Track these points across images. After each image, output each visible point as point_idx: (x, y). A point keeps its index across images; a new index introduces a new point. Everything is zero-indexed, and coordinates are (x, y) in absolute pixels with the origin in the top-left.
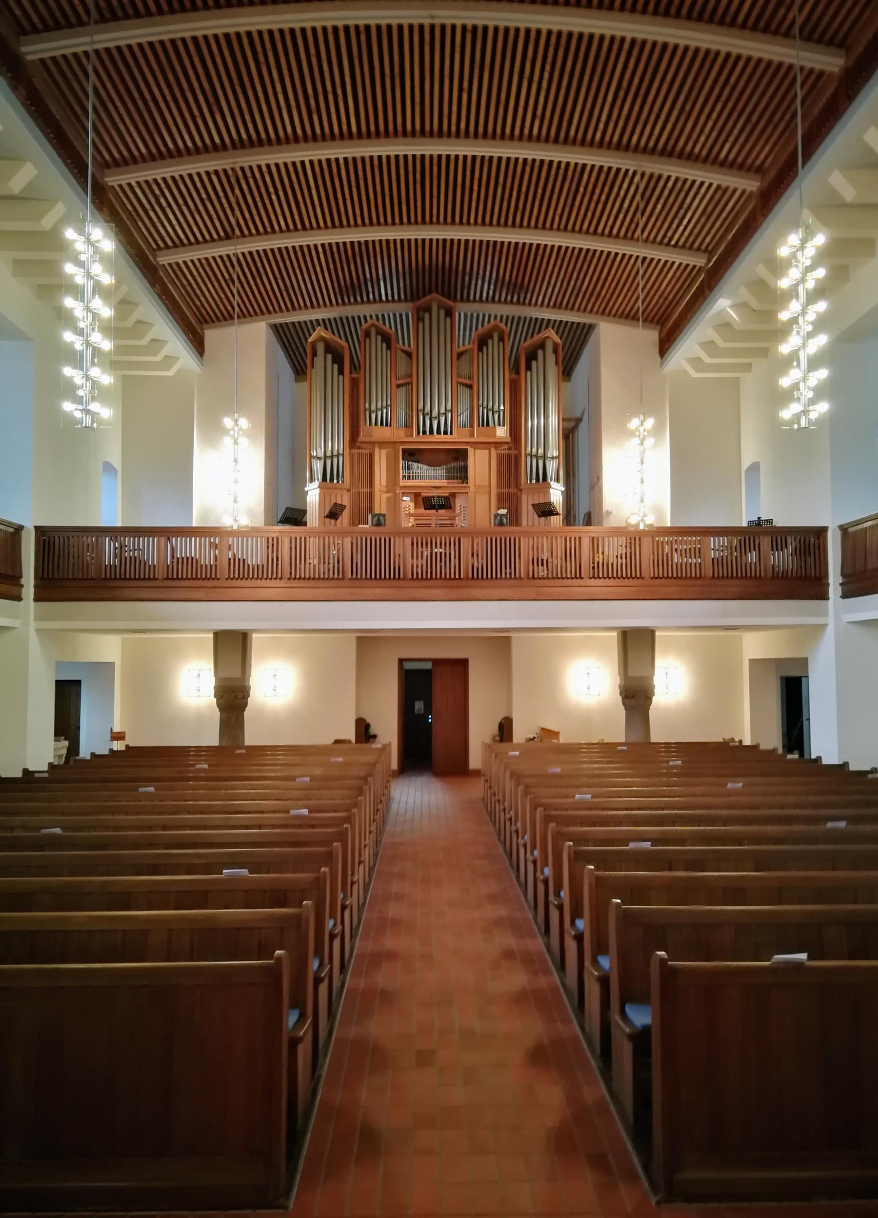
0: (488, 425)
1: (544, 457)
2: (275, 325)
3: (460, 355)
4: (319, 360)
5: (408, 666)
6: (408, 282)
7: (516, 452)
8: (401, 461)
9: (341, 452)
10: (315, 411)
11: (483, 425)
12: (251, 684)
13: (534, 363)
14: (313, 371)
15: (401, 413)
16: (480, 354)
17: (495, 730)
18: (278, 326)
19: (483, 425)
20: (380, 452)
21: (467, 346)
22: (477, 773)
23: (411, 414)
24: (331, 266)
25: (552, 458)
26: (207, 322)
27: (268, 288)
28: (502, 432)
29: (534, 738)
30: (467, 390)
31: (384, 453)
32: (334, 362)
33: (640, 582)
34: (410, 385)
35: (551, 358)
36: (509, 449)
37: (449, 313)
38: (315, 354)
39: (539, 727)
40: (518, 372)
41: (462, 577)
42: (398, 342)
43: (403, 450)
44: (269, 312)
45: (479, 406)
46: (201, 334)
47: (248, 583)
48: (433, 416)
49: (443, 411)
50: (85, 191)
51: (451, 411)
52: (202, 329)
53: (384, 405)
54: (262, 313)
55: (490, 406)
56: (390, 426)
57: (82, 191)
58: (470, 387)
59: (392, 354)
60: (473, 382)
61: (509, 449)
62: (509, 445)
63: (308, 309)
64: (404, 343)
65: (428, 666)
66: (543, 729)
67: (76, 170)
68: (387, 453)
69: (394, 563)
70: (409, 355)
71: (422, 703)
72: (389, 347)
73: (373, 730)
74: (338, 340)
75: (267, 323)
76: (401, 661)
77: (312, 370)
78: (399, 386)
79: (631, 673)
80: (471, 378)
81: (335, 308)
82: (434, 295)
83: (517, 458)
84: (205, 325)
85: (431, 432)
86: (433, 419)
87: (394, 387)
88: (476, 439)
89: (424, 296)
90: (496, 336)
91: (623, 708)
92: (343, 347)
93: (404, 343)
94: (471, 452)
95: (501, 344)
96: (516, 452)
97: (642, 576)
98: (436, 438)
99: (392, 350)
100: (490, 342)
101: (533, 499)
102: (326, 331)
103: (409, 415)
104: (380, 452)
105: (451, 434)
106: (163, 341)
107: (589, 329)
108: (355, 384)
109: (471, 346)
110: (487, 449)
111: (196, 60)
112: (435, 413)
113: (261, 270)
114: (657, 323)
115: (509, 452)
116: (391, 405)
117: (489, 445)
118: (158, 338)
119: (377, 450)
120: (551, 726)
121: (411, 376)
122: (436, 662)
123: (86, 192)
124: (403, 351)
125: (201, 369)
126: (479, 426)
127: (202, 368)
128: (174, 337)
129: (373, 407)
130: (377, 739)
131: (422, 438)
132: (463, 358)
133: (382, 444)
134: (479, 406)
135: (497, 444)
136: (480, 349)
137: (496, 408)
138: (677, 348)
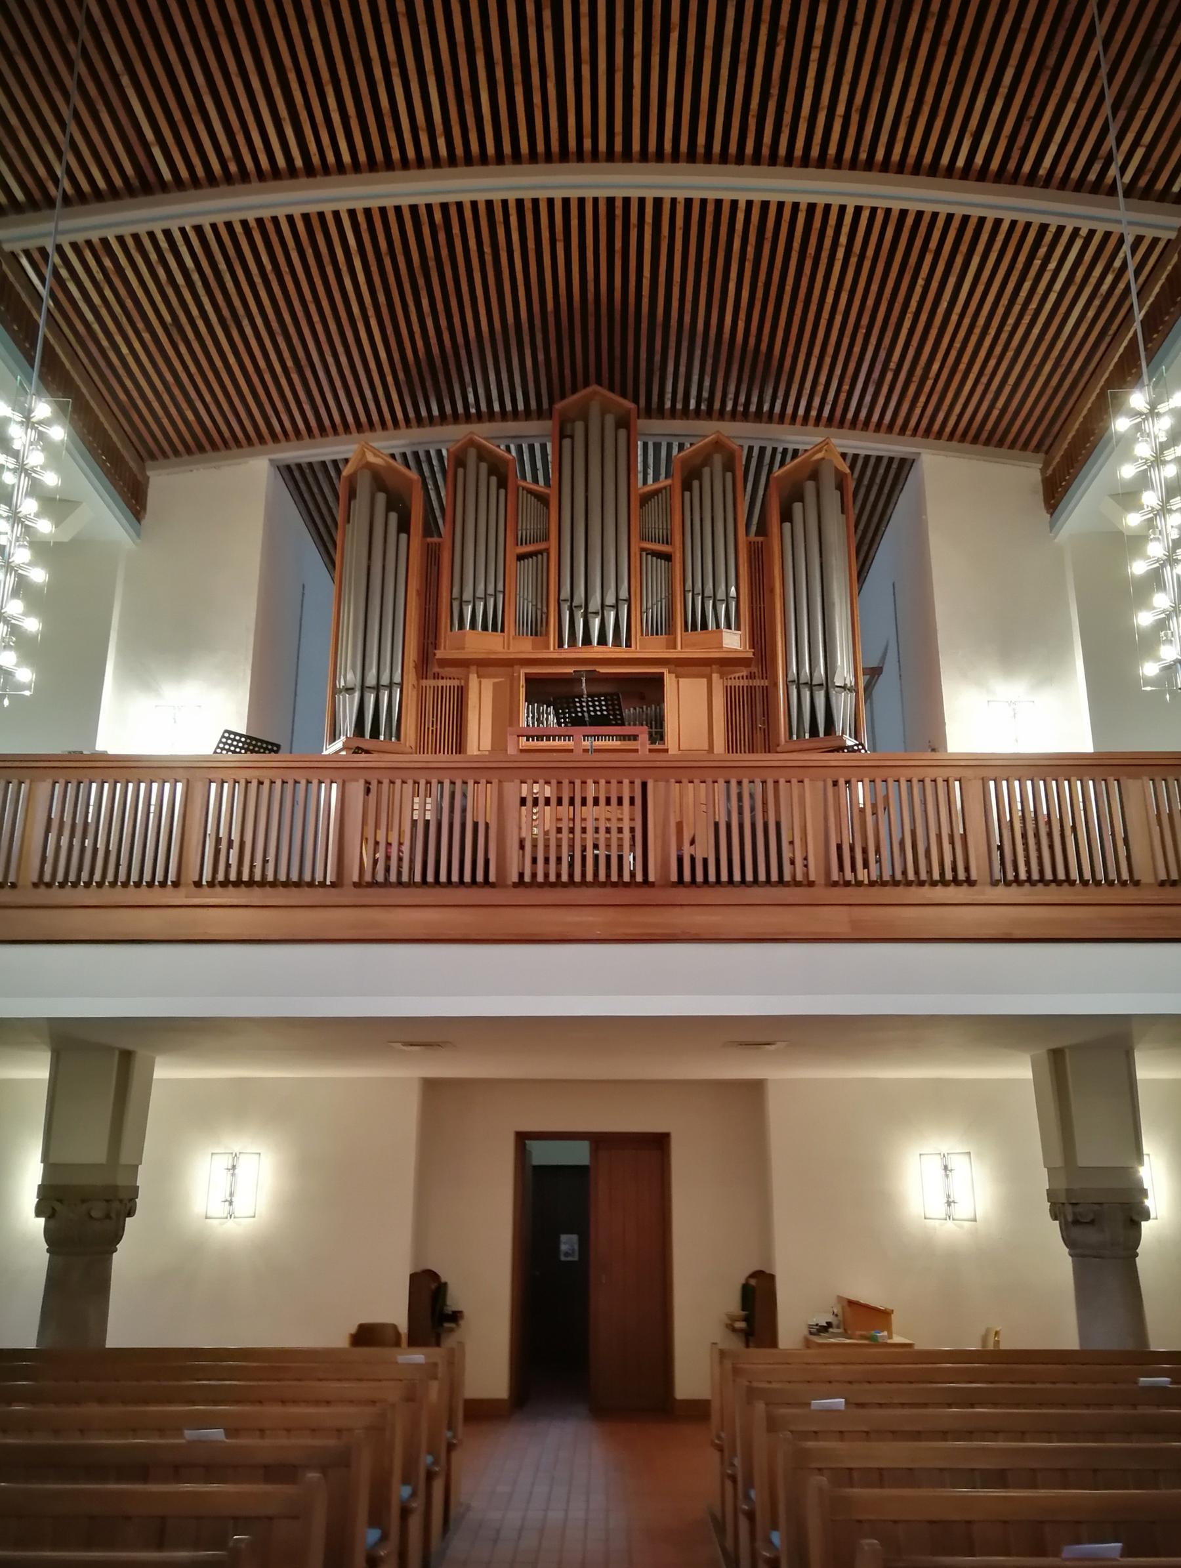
0: (704, 626)
1: (827, 685)
2: (288, 467)
3: (645, 499)
4: (361, 506)
5: (544, 1154)
6: (541, 357)
7: (765, 683)
8: (523, 705)
9: (397, 679)
10: (346, 611)
11: (694, 628)
12: (42, 1164)
13: (797, 507)
14: (349, 527)
15: (524, 602)
16: (687, 494)
17: (732, 1303)
18: (294, 467)
19: (694, 628)
20: (480, 683)
21: (663, 482)
22: (698, 1411)
23: (545, 610)
24: (382, 298)
25: (844, 687)
26: (153, 457)
27: (262, 364)
28: (733, 641)
29: (829, 1325)
30: (662, 563)
31: (488, 685)
32: (389, 508)
33: (1130, 894)
34: (545, 554)
35: (832, 499)
36: (751, 676)
37: (623, 423)
38: (352, 495)
39: (840, 1298)
40: (762, 530)
41: (651, 878)
42: (524, 478)
43: (530, 680)
45: (685, 592)
46: (139, 477)
47: (91, 896)
48: (591, 609)
49: (610, 600)
50: (31, 361)
51: (629, 601)
52: (143, 470)
53: (491, 590)
55: (709, 590)
56: (502, 631)
57: (26, 363)
58: (668, 557)
61: (751, 676)
62: (749, 669)
63: (350, 433)
64: (535, 480)
65: (579, 1154)
66: (851, 1303)
67: (108, 465)
68: (495, 685)
69: (464, 810)
70: (543, 499)
71: (574, 1238)
72: (502, 484)
73: (457, 1298)
74: (403, 469)
75: (271, 461)
76: (522, 1138)
77: (347, 526)
78: (521, 557)
79: (1085, 1159)
80: (668, 541)
81: (404, 430)
82: (594, 387)
83: (768, 695)
84: (149, 463)
85: (587, 640)
86: (589, 615)
87: (511, 558)
88: (678, 653)
89: (574, 390)
90: (718, 460)
91: (1066, 1250)
92: (410, 480)
93: (535, 480)
94: (669, 680)
96: (765, 683)
97: (1136, 877)
98: (596, 651)
99: (509, 490)
100: (706, 471)
101: (1029, 119)
103: (542, 613)
104: (480, 683)
105: (628, 645)
106: (69, 501)
107: (903, 467)
108: (432, 557)
110: (702, 676)
112: (595, 604)
113: (241, 311)
114: (1037, 449)
115: (750, 683)
116: (504, 592)
117: (707, 670)
118: (71, 499)
119: (473, 680)
120: (869, 1294)
121: (546, 538)
122: (599, 1141)
123: (32, 367)
124: (530, 492)
126: (686, 629)
127: (139, 541)
129: (468, 595)
130: (462, 1323)
131: (567, 653)
132: (654, 501)
133: (484, 665)
134: (685, 592)
135: (727, 663)
136: (687, 486)
137: (721, 594)
138: (1093, 471)
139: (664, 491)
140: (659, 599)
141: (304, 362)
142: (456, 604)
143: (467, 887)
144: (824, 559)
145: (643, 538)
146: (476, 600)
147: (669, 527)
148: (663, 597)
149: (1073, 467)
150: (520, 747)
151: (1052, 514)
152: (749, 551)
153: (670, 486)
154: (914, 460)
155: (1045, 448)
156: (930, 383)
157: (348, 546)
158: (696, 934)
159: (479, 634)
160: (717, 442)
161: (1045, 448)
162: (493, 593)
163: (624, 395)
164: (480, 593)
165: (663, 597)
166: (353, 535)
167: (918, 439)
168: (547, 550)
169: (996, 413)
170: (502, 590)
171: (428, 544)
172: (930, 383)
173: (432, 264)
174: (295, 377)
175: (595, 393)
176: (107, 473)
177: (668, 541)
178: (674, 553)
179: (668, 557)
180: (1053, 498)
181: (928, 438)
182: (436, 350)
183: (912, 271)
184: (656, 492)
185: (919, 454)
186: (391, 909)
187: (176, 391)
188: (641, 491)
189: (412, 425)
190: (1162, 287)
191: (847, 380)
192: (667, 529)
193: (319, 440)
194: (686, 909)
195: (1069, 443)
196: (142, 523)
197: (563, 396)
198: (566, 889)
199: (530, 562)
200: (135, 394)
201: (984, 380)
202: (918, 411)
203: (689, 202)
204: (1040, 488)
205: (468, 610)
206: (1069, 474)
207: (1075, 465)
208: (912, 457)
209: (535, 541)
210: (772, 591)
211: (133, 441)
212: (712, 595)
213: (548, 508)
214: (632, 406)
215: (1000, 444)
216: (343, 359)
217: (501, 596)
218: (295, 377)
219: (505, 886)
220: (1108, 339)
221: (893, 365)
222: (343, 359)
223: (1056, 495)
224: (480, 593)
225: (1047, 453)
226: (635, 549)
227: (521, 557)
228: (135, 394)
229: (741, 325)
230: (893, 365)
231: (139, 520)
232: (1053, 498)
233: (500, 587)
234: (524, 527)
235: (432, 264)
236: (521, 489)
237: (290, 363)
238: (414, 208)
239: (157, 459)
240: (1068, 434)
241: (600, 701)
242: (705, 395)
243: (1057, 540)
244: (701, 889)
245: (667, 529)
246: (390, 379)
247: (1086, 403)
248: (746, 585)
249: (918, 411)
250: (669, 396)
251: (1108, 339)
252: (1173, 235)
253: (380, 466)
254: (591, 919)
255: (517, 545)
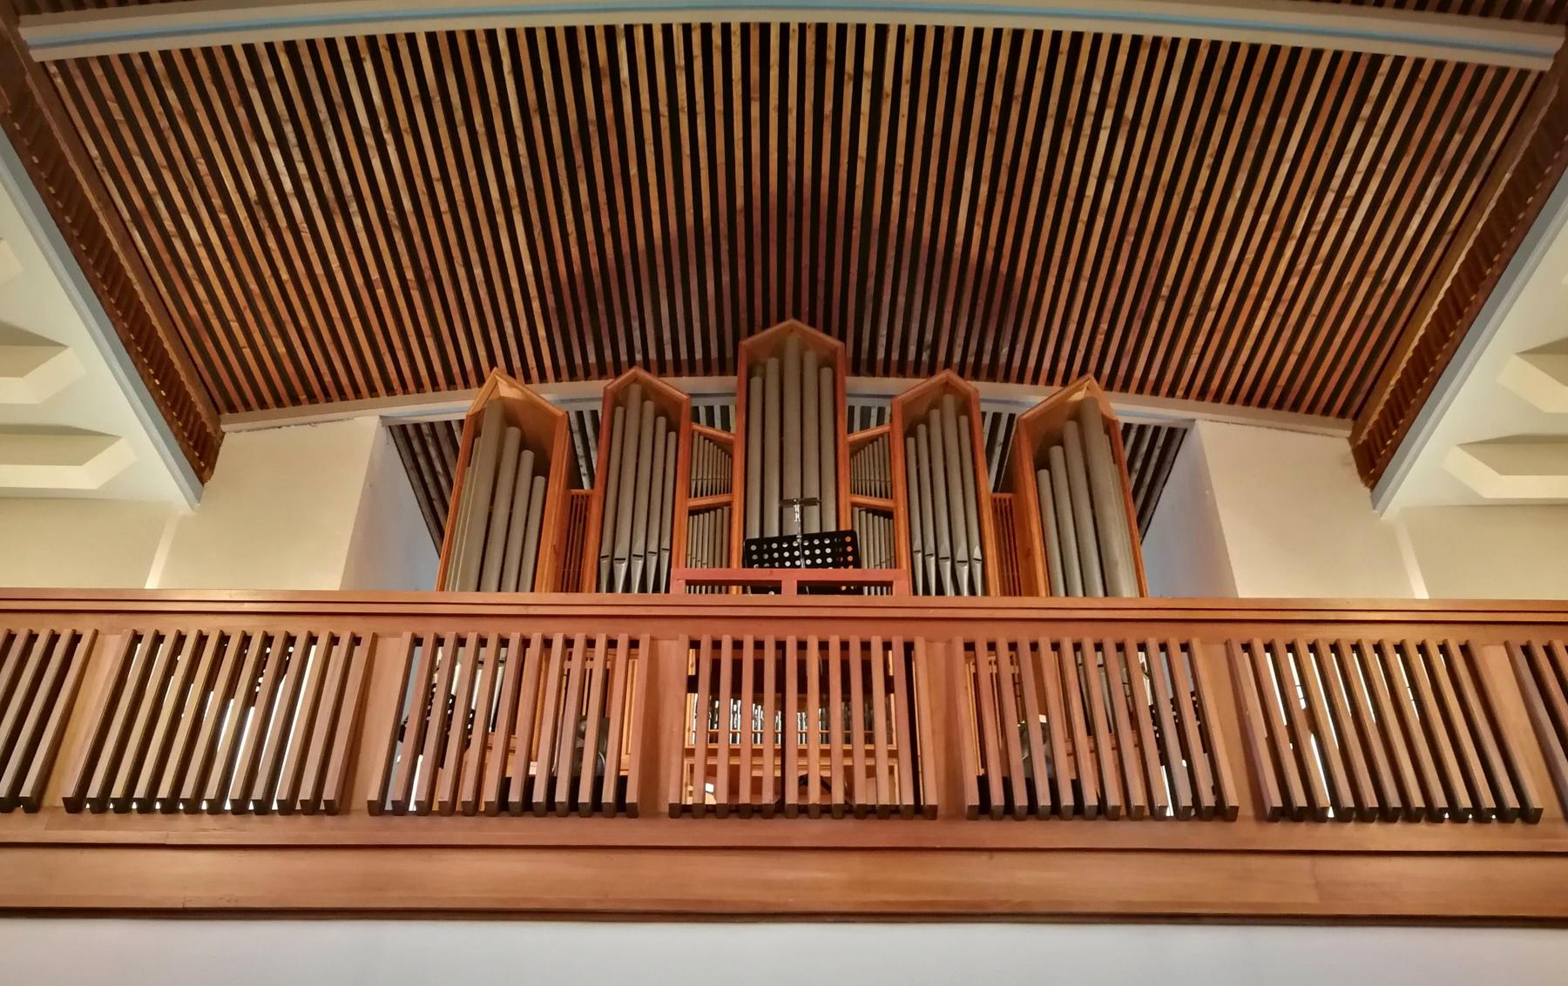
2: (403, 428)
3: (857, 448)
4: (486, 446)
6: (726, 278)
16: (911, 441)
26: (232, 408)
27: (375, 275)
30: (880, 521)
44: (390, 390)
46: (210, 429)
52: (217, 423)
53: (653, 547)
54: (373, 392)
58: (888, 514)
59: (681, 440)
60: (896, 501)
72: (672, 427)
78: (693, 512)
80: (887, 493)
82: (790, 322)
87: (681, 513)
89: (766, 325)
90: (949, 402)
95: (964, 420)
102: (511, 379)
106: (113, 436)
107: (1174, 437)
108: (576, 514)
109: (885, 428)
111: (430, 342)
114: (1342, 414)
116: (671, 550)
121: (728, 489)
125: (191, 506)
128: (62, 293)
129: (622, 550)
136: (910, 432)
137: (961, 554)
139: (880, 439)
140: (878, 562)
141: (428, 274)
142: (605, 562)
143: (582, 816)
144: (1096, 510)
145: (854, 491)
146: (633, 558)
147: (888, 479)
148: (883, 560)
149: (1402, 416)
150: (686, 746)
151: (1372, 488)
152: (995, 510)
153: (889, 433)
154: (1185, 431)
155: (1353, 410)
156: (1211, 315)
157: (466, 486)
158: (1021, 904)
159: (636, 596)
160: (947, 383)
161: (1353, 410)
162: (656, 550)
163: (827, 331)
164: (639, 548)
165: (883, 560)
166: (473, 477)
167: (1191, 401)
168: (729, 504)
169: (1293, 359)
170: (668, 547)
171: (573, 497)
172: (1211, 315)
173: (593, 129)
174: (416, 295)
175: (791, 330)
176: (160, 402)
177: (887, 493)
178: (896, 508)
179: (888, 514)
180: (1373, 465)
181: (1203, 400)
182: (595, 263)
183: (1197, 145)
184: (873, 440)
185: (1194, 420)
186: (436, 854)
187: (262, 307)
188: (799, 748)
189: (563, 378)
190: (1535, 139)
191: (1107, 316)
192: (886, 481)
193: (445, 393)
194: (998, 857)
195: (1393, 391)
196: (206, 484)
197: (751, 332)
198: (769, 821)
199: (707, 517)
200: (208, 308)
201: (1281, 309)
202: (1193, 360)
203: (920, 31)
204: (1351, 458)
205: (622, 569)
206: (1396, 426)
207: (1406, 412)
208: (1182, 426)
209: (713, 492)
210: (1029, 554)
211: (206, 379)
212: (949, 555)
213: (731, 456)
214: (838, 343)
215: (1295, 407)
216: (478, 271)
217: (667, 554)
218: (416, 295)
219: (654, 814)
220: (1446, 239)
221: (1165, 291)
222: (478, 271)
223: (1378, 461)
224: (639, 548)
225: (1355, 417)
226: (846, 498)
227: (693, 512)
228: (208, 308)
229: (977, 232)
230: (1165, 291)
231: (202, 481)
232: (1373, 465)
233: (666, 544)
234: (700, 477)
235: (593, 129)
236: (696, 434)
237: (410, 275)
238: (571, 32)
239: (238, 412)
240: (1391, 379)
241: (822, 547)
242: (929, 337)
243: (1382, 519)
244: (1026, 822)
245: (886, 481)
246: (536, 305)
247: (1400, 363)
248: (994, 545)
249: (1193, 360)
250: (882, 341)
251: (1446, 239)
252: (1546, 65)
253: (514, 399)
254: (820, 875)
255: (690, 497)
